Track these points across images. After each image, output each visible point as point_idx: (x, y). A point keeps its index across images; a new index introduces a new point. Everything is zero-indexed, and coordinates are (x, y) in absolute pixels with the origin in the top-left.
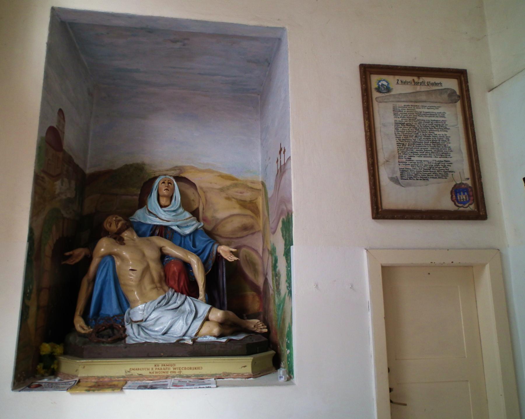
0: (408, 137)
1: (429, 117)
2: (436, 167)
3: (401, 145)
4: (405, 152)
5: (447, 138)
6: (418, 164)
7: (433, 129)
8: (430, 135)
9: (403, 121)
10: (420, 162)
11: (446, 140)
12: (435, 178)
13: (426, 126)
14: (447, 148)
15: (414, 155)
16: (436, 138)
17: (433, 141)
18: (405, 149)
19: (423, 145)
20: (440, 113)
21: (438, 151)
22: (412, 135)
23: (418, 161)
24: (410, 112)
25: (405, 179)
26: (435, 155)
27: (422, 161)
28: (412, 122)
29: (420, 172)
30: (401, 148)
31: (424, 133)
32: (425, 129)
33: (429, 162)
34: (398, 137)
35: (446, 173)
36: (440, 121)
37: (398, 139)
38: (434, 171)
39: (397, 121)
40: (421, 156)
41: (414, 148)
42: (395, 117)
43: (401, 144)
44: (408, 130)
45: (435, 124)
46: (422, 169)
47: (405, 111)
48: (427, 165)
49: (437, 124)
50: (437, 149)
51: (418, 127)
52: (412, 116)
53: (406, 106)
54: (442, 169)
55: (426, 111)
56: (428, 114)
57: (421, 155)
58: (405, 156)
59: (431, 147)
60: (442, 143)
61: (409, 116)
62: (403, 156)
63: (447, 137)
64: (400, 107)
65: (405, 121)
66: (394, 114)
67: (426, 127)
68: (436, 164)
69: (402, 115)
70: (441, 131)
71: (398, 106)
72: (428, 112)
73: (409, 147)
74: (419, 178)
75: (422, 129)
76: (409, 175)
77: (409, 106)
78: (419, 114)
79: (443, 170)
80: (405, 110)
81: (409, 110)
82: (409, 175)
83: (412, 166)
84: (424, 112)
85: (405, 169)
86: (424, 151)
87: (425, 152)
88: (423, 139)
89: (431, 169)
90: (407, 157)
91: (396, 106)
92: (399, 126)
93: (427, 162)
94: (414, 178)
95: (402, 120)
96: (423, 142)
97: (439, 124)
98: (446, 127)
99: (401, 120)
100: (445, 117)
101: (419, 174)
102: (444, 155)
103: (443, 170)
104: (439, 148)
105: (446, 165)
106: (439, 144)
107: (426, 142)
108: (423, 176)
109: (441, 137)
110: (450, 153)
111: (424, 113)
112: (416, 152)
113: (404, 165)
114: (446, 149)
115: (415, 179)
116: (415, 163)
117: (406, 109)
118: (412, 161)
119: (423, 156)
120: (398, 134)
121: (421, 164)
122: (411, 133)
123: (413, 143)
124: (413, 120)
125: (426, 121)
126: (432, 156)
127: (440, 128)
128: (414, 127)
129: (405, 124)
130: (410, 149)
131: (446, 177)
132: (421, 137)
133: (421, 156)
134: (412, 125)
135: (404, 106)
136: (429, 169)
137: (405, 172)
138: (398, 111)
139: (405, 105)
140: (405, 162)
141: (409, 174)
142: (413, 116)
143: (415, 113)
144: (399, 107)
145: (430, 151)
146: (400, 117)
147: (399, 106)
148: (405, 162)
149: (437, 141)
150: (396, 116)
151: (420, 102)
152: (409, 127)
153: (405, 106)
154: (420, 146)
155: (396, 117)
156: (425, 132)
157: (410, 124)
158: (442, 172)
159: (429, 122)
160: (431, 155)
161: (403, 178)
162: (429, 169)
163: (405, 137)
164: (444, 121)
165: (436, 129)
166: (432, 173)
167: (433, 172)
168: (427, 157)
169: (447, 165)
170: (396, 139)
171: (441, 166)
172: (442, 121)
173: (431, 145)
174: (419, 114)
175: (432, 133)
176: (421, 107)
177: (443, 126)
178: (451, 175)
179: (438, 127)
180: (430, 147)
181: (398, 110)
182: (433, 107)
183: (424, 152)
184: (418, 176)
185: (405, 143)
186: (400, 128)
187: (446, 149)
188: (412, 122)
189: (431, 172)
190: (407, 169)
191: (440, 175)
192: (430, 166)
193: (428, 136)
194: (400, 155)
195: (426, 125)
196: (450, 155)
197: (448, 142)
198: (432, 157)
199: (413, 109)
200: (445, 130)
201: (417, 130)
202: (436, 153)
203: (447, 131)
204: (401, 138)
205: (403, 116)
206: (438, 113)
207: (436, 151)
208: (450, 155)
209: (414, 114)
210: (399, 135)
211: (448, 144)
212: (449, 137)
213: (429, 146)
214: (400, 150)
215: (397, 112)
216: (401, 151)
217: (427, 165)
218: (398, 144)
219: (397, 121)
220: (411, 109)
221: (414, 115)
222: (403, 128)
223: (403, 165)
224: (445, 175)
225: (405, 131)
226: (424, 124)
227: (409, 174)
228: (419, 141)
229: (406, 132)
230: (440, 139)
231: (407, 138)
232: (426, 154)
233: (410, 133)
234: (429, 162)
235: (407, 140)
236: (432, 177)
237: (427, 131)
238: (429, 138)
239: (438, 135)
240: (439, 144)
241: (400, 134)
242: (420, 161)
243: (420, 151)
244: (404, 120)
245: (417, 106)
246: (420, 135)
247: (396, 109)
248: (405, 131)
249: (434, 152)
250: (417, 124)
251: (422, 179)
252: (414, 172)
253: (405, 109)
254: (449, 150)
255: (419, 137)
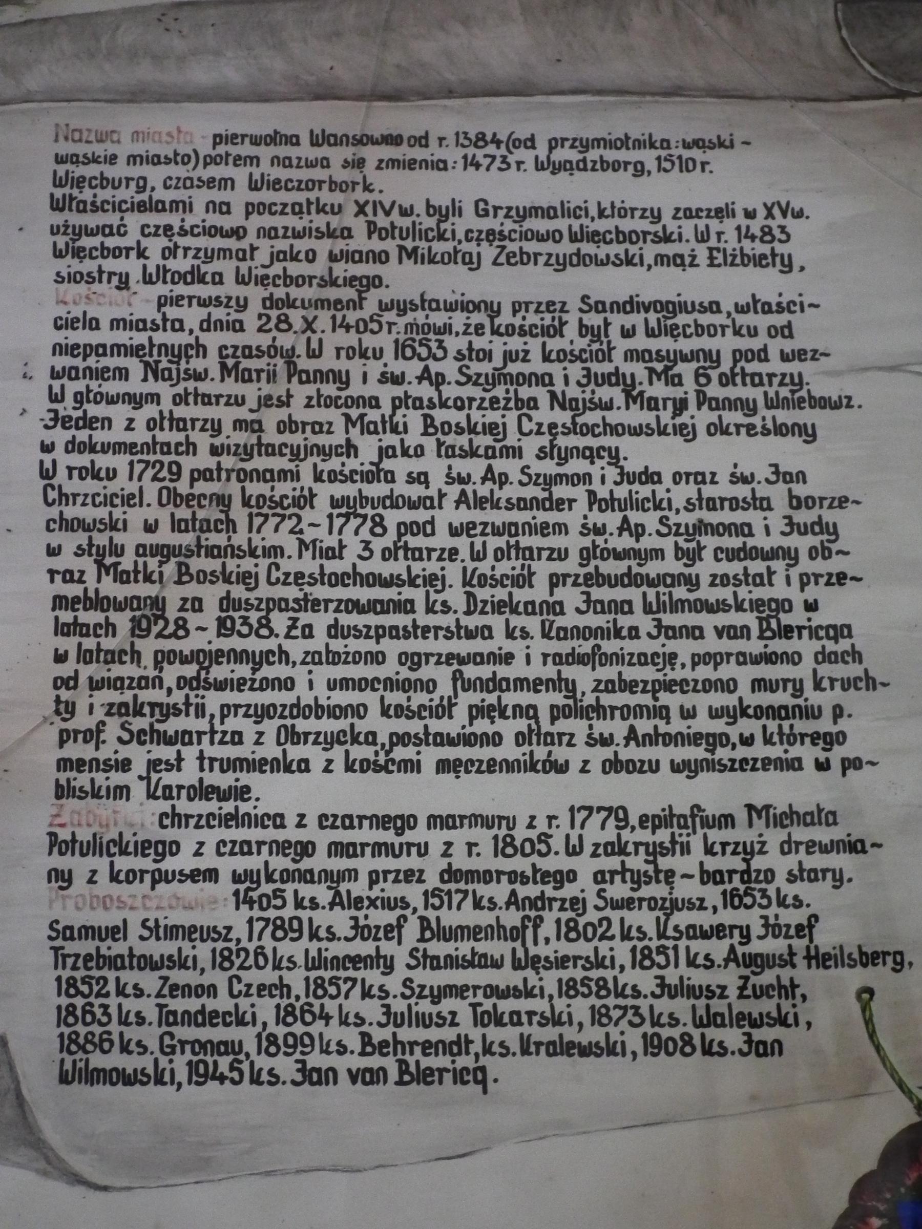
0: (239, 513)
1: (562, 264)
2: (628, 904)
3: (122, 620)
4: (172, 711)
5: (803, 516)
6: (339, 864)
7: (608, 406)
8: (561, 491)
9: (178, 326)
10: (389, 836)
11: (794, 541)
12: (585, 1051)
13: (499, 377)
14: (807, 647)
15: (295, 752)
16: (650, 520)
17: (587, 555)
18: (171, 673)
19: (446, 608)
20: (720, 213)
21: (668, 686)
22: (284, 488)
23: (348, 822)
24: (298, 210)
25: (127, 1079)
26: (606, 741)
27: (406, 822)
28: (309, 325)
29: (373, 977)
30: (114, 657)
31: (475, 467)
32: (493, 416)
33: (521, 833)
34: (67, 525)
35: (768, 977)
36: (714, 307)
37: (80, 552)
38: (583, 948)
39: (93, 324)
40: (400, 753)
41: (313, 658)
42: (73, 278)
43: (119, 607)
44: (239, 424)
45: (640, 342)
46: (393, 931)
47: (224, 208)
48: (486, 877)
49: (665, 343)
50: (643, 659)
51: (387, 393)
52: (311, 257)
53: (246, 149)
54: (704, 919)
55: (523, 200)
56: (554, 236)
57: (401, 739)
58: (153, 765)
59: (564, 634)
60: (724, 580)
61: (276, 257)
62: (125, 765)
63: (796, 503)
64: (156, 160)
65: (207, 325)
66: (61, 241)
67: (499, 391)
68: (614, 863)
69: (170, 252)
70: (718, 429)
71: (124, 150)
72: (549, 213)
73: (226, 644)
74: (342, 1049)
75: (440, 415)
76: (189, 1018)
77: (294, 141)
78: (413, 232)
79: (719, 931)
80: (218, 196)
81: (275, 185)
82: (189, 1018)
83: (242, 900)
84: (482, 209)
85: (135, 930)
86: (445, 688)
87: (466, 699)
88: (442, 539)
89: (548, 929)
90: (189, 774)
91: (99, 149)
92: (113, 387)
93: (483, 837)
94: (263, 1062)
95: (172, 312)
96: (453, 573)
97: (705, 343)
98: (799, 382)
99: (150, 313)
100: (788, 266)
101: (354, 1004)
102: (747, 741)
103: (719, 931)
104: (684, 648)
105: (770, 875)
106: (680, 592)
107: (483, 581)
108: (406, 1034)
109: (712, 504)
110: (838, 712)
111: (487, 224)
112: (335, 712)
113: (132, 876)
114: (793, 659)
115: (275, 1079)
116: (306, 849)
117: (241, 175)
118: (260, 821)
119: (430, 755)
120: (91, 486)
121: (385, 863)
122: (278, 463)
123: (292, 592)
124: (321, 303)
125: (505, 318)
126: (575, 756)
127: (714, 390)
128: (329, 389)
129: (212, 363)
130: (244, 670)
131: (766, 1034)
132: (421, 515)
133: (400, 753)
134: (304, 363)
135: (218, 139)
136: (517, 934)
137: (129, 977)
138: (118, 207)
139: (232, 139)
140: (143, 847)
141: (193, 1004)
142: (333, 258)
143: (359, 226)
144: (132, 159)
145: (536, 685)
146: (136, 275)
147: (139, 149)
148: (143, 847)
149: (659, 554)
150: (90, 266)
151: (451, 93)
152: (251, 392)
153: (221, 149)
154: (394, 632)
155: (90, 279)
156: (490, 454)
157: (273, 350)
158: (709, 963)
159: (558, 331)
160: (549, 739)
161: (98, 1060)
162: (517, 934)
163: (183, 513)
164: (767, 308)
165: (653, 404)
166: (550, 979)
167: (562, 962)
168: (492, 766)
169: (791, 862)
170: (53, 552)
171: (687, 889)
172: (741, 309)
173: (557, 608)
174: (424, 235)
175: (591, 455)
176: (453, 155)
177: (753, 367)
178: (856, 1007)
179: (677, 380)
180: (545, 635)
181: (126, 194)
182: (624, 142)
183: (445, 709)
184: (334, 1032)
185: (173, 595)
186: (120, 413)
187: (793, 659)
188: (309, 325)
189: (534, 962)
190: (172, 932)
191: (682, 1006)
192: (531, 890)
193: (522, 504)
194: (86, 751)
195: (509, 357)
196: (830, 740)
197: (820, 566)
198: (562, 768)
199: (341, 175)
200: (784, 416)
201: (369, 429)
202: (626, 712)
203: (809, 434)
204: (130, 539)
205: (181, 264)
206: (689, 214)
207: (630, 686)
208: (830, 740)
209: (347, 233)
210: (109, 501)
211: (812, 592)
212: (843, 502)
213: (533, 624)
214: (95, 685)
215: (113, 219)
216: (109, 696)
217: (486, 877)
218: (66, 617)
219: (93, 324)
220: (318, 174)
221: (339, 245)
222: (265, 166)
223: (114, 878)
224: (755, 1007)
225: (191, 448)
226: (488, 355)
227: (193, 1004)
228: (398, 567)
229: (204, 461)
230: (701, 527)
231: (207, 526)
232: (482, 726)
233: (260, 463)
234: (521, 833)
235: (212, 552)
236: (550, 1033)
237: (512, 440)
238: (544, 529)
239: (677, 478)
240: (680, 592)
241: (122, 484)
242: (383, 822)
243: (395, 698)
244: (192, 316)
245: (393, 140)
246: (401, 488)
247: (104, 182)
248: (191, 448)
249: (607, 700)
250: (378, 354)
251: (390, 1064)
252: (269, 976)
253: (227, 183)
254: (825, 670)
255: (392, 517)
